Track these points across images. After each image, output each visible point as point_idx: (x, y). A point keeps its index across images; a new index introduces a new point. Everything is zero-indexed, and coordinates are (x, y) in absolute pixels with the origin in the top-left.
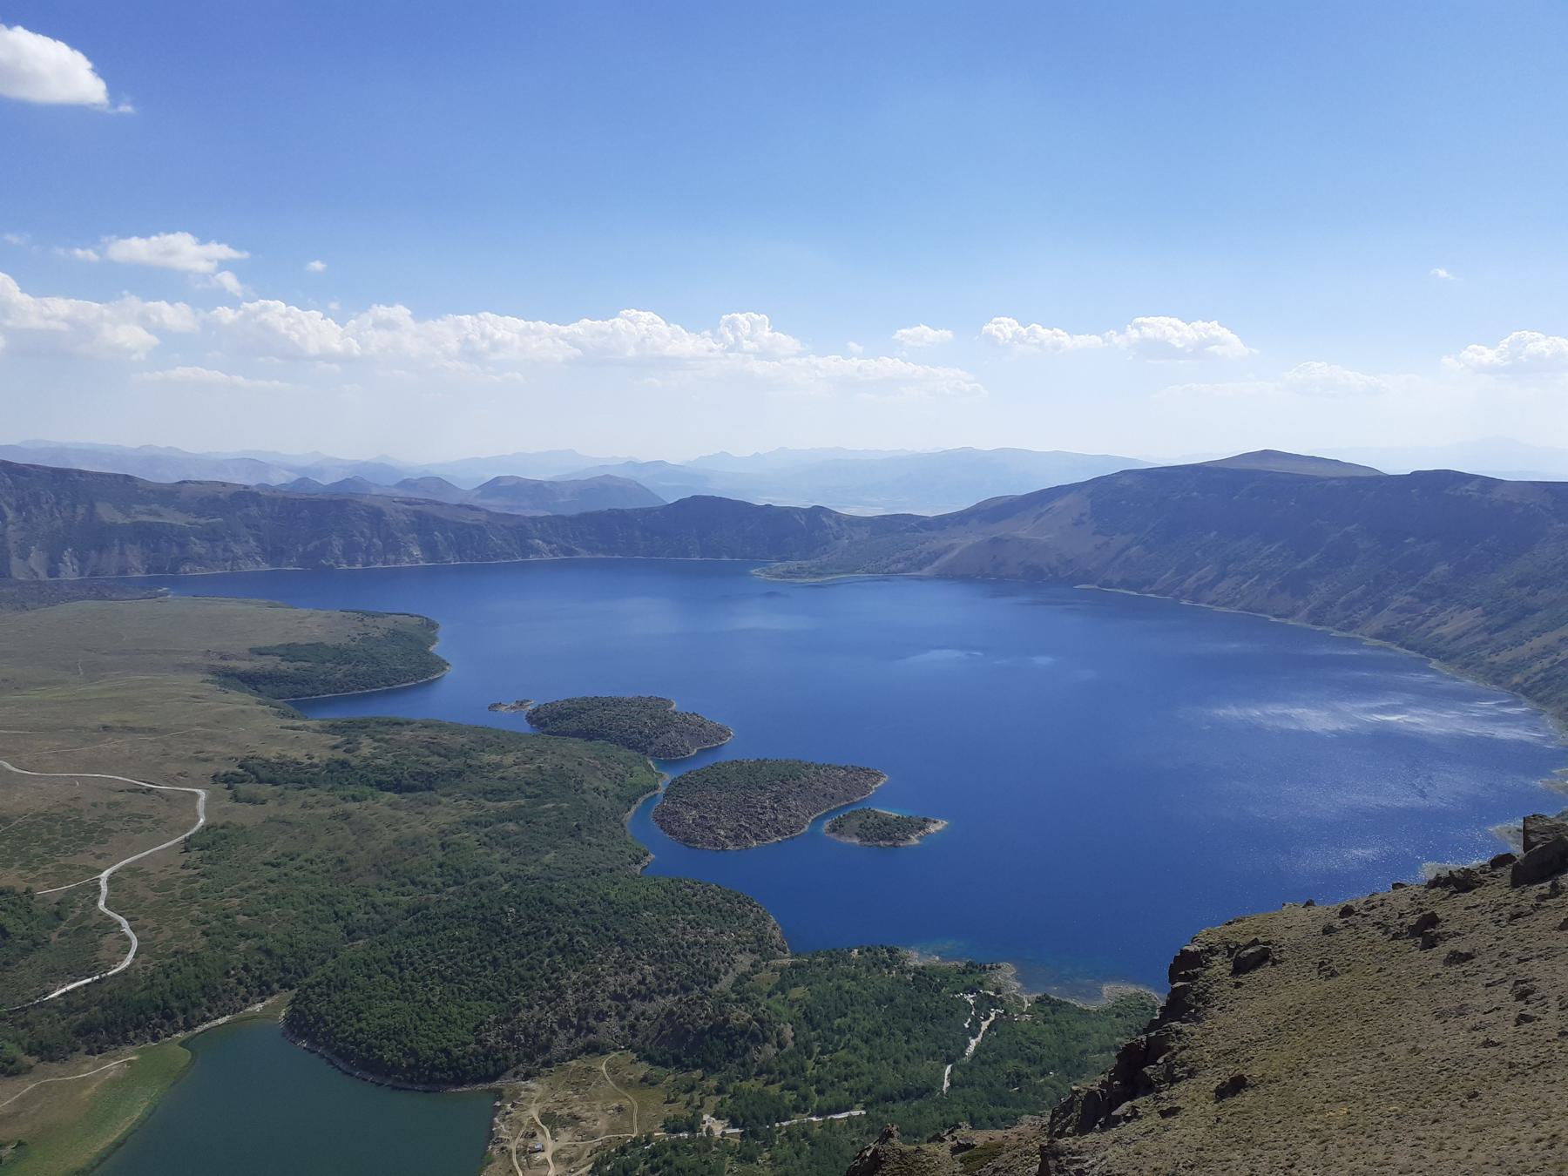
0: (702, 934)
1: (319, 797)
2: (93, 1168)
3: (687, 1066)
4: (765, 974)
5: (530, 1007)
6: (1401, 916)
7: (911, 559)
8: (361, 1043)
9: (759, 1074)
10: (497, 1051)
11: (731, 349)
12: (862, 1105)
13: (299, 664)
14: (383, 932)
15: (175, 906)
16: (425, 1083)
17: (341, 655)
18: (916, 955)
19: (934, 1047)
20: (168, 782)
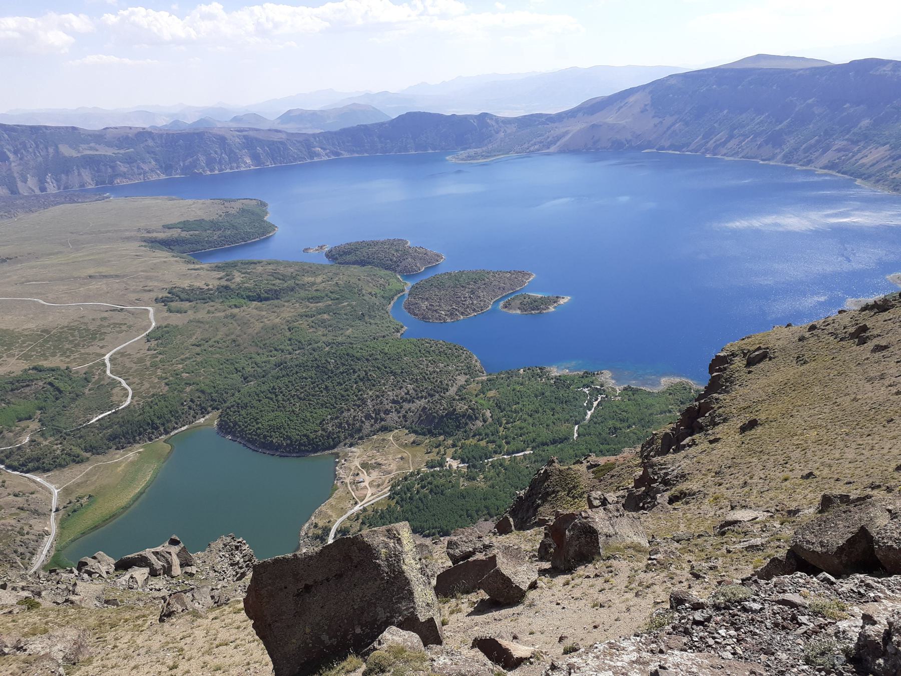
0: (437, 367)
1: (215, 307)
2: (130, 505)
3: (436, 434)
4: (473, 385)
5: (349, 410)
6: (845, 328)
7: (543, 142)
8: (260, 435)
9: (474, 436)
10: (333, 434)
11: (421, 15)
12: (531, 448)
13: (191, 233)
14: (263, 377)
15: (148, 370)
16: (297, 453)
17: (215, 225)
18: (555, 370)
19: (568, 417)
20: (131, 304)
